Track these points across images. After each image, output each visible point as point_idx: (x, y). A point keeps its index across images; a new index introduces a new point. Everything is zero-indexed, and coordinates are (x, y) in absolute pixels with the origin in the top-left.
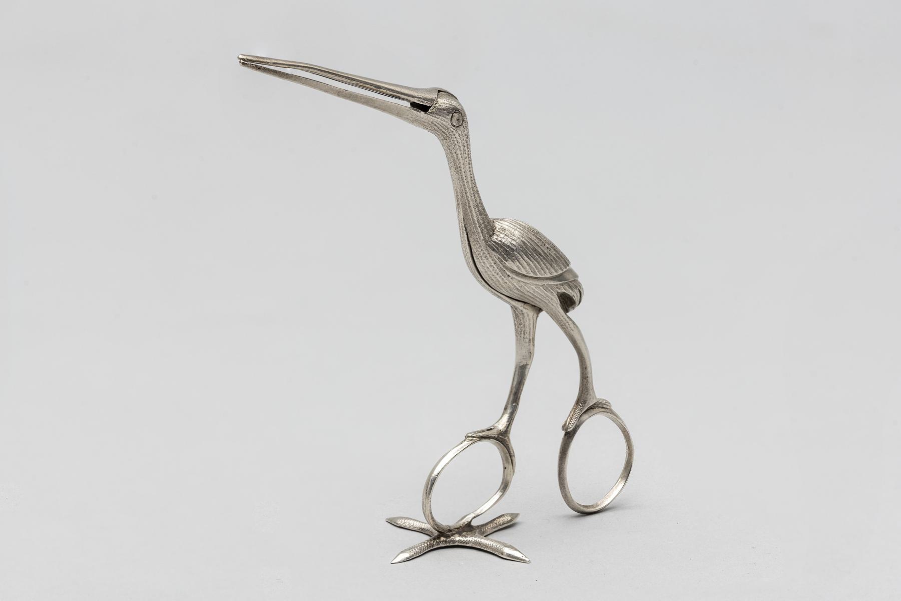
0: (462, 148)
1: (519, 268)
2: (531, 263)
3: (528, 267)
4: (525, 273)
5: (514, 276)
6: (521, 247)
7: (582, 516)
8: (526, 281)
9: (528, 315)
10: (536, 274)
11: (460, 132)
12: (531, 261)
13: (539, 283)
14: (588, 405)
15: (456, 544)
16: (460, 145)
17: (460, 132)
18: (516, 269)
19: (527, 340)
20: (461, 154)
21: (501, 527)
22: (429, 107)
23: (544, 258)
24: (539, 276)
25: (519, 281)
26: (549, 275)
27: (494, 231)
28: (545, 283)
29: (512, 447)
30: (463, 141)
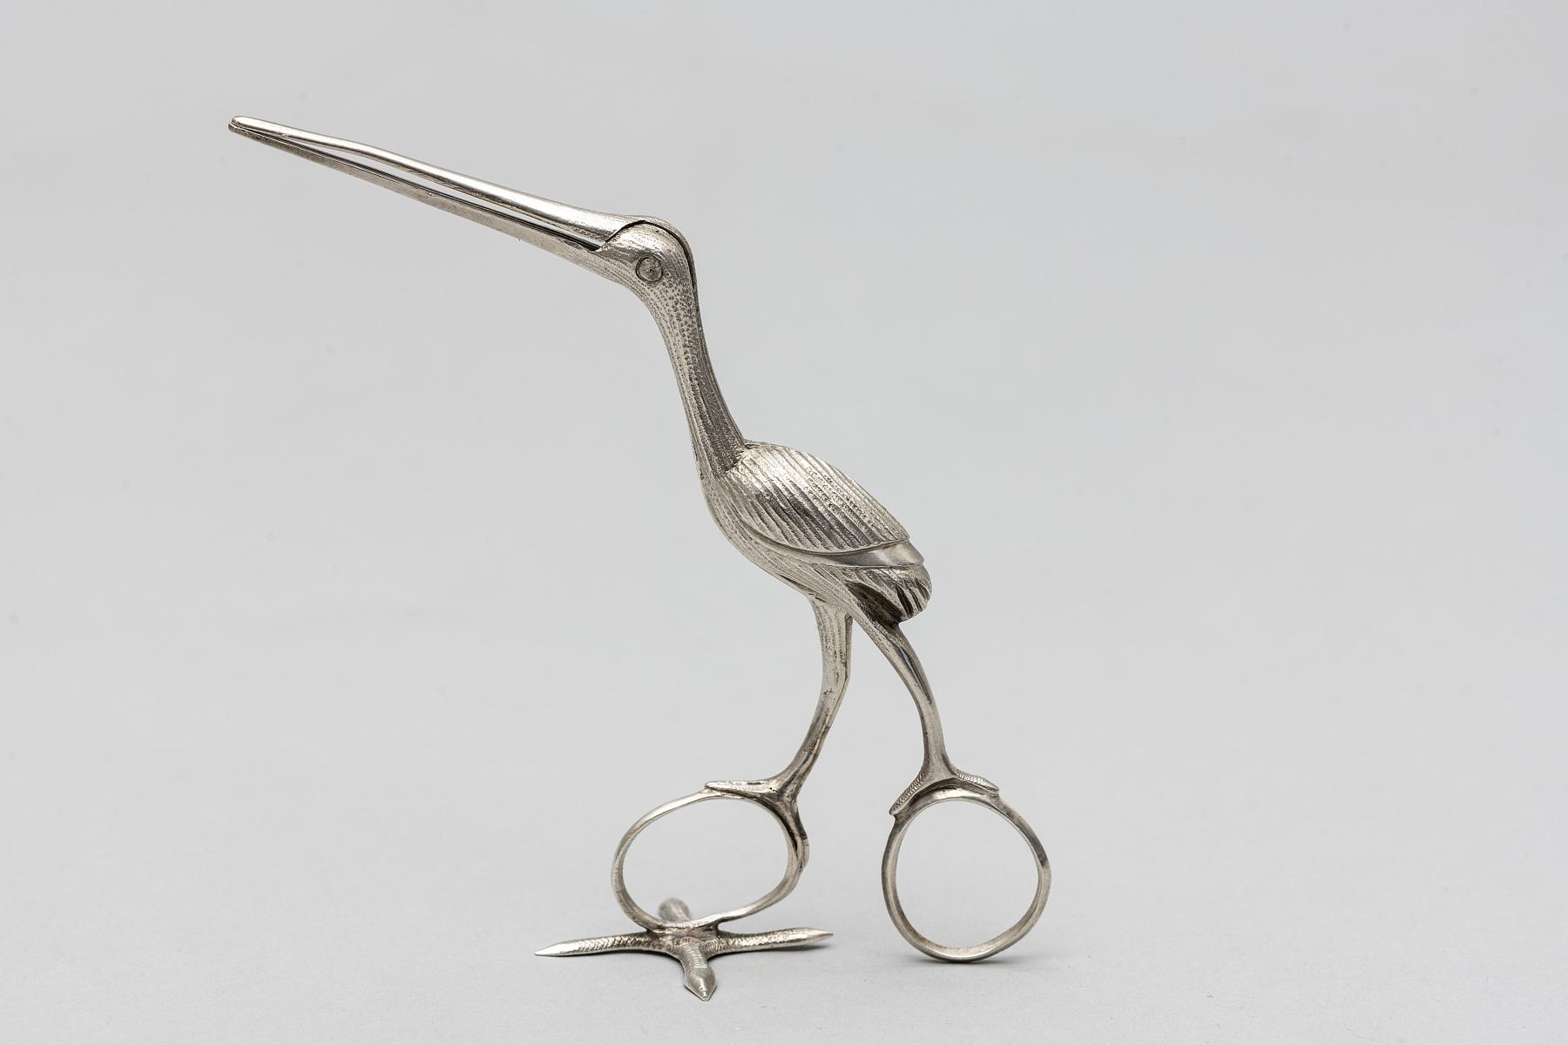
0: (667, 318)
1: (762, 528)
2: (785, 524)
3: (778, 530)
4: (773, 538)
5: (758, 541)
6: (768, 495)
7: (936, 962)
8: (780, 552)
9: (826, 612)
10: (797, 544)
11: (658, 293)
12: (783, 520)
13: (807, 559)
14: (930, 780)
15: (663, 950)
16: (663, 312)
17: (658, 293)
18: (757, 528)
19: (832, 653)
20: (668, 328)
21: (775, 946)
22: (598, 247)
23: (813, 520)
24: (802, 547)
25: (769, 550)
26: (822, 550)
27: (736, 461)
28: (819, 561)
29: (906, 830)
30: (667, 308)
